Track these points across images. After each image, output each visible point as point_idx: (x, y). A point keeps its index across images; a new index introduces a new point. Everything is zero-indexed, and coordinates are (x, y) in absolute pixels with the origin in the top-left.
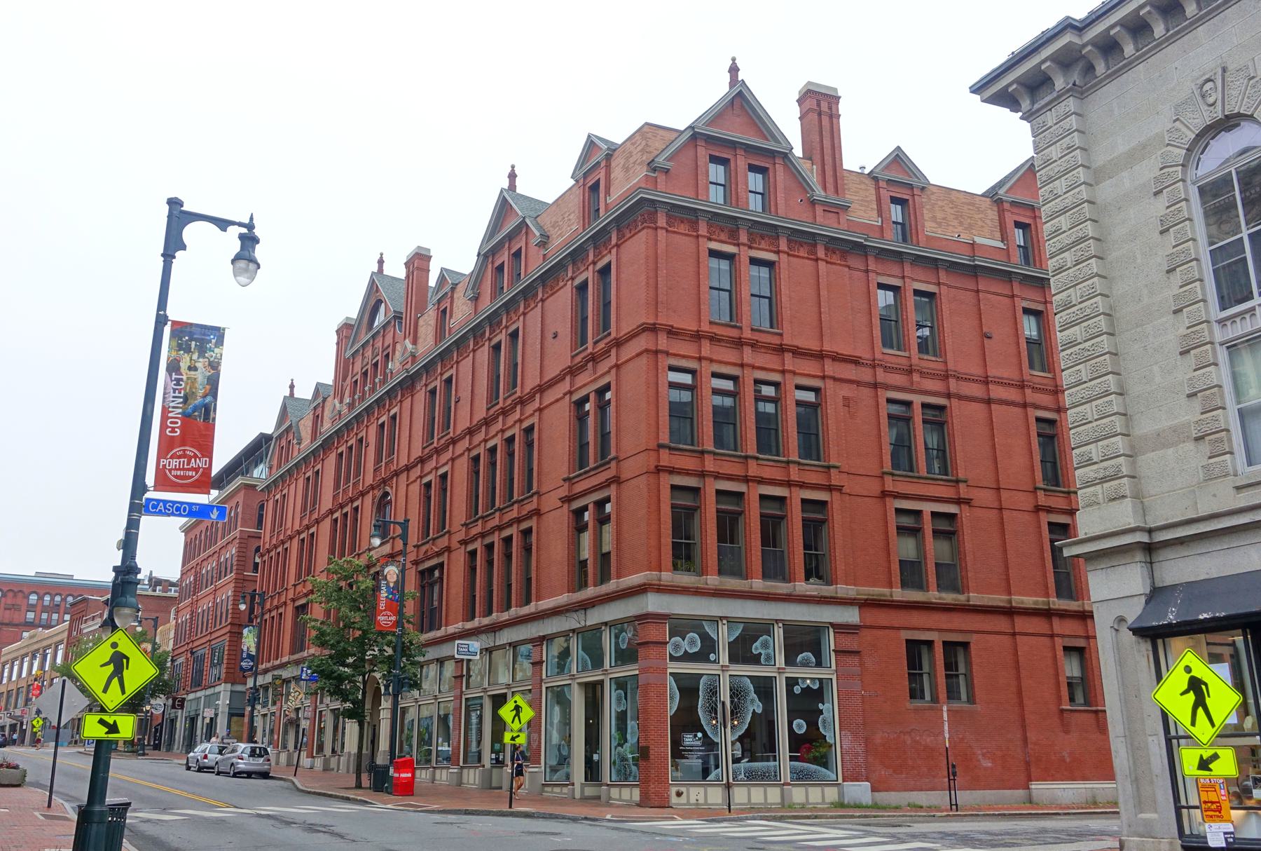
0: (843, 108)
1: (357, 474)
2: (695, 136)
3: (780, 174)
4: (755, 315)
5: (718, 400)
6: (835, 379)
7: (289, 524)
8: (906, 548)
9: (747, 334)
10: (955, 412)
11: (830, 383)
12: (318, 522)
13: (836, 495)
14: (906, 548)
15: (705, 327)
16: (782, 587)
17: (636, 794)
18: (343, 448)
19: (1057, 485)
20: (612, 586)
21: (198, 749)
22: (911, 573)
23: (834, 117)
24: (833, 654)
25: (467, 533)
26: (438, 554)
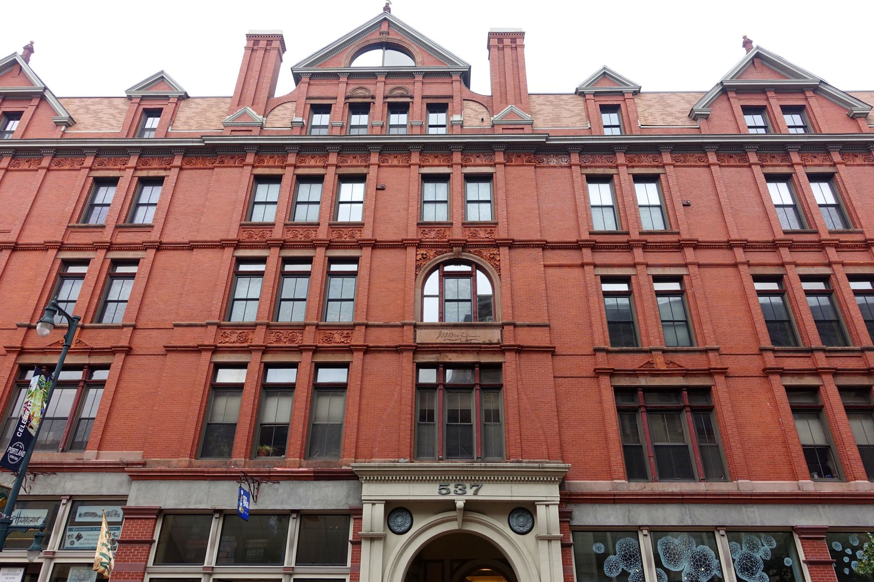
0: (527, 41)
2: (725, 90)
3: (814, 103)
4: (830, 222)
5: (813, 301)
6: (700, 266)
8: (809, 433)
9: (825, 236)
10: (697, 283)
11: (694, 270)
13: (720, 380)
14: (809, 433)
15: (780, 236)
16: (828, 487)
19: (847, 345)
22: (820, 460)
24: (805, 568)
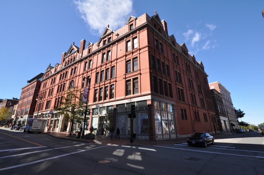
1: (66, 77)
7: (47, 87)
12: (67, 81)
17: (147, 137)
18: (62, 73)
20: (135, 95)
21: (16, 126)
23: (129, 42)
25: (95, 86)
26: (50, 99)
